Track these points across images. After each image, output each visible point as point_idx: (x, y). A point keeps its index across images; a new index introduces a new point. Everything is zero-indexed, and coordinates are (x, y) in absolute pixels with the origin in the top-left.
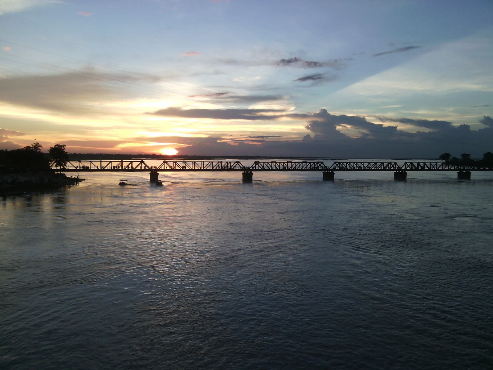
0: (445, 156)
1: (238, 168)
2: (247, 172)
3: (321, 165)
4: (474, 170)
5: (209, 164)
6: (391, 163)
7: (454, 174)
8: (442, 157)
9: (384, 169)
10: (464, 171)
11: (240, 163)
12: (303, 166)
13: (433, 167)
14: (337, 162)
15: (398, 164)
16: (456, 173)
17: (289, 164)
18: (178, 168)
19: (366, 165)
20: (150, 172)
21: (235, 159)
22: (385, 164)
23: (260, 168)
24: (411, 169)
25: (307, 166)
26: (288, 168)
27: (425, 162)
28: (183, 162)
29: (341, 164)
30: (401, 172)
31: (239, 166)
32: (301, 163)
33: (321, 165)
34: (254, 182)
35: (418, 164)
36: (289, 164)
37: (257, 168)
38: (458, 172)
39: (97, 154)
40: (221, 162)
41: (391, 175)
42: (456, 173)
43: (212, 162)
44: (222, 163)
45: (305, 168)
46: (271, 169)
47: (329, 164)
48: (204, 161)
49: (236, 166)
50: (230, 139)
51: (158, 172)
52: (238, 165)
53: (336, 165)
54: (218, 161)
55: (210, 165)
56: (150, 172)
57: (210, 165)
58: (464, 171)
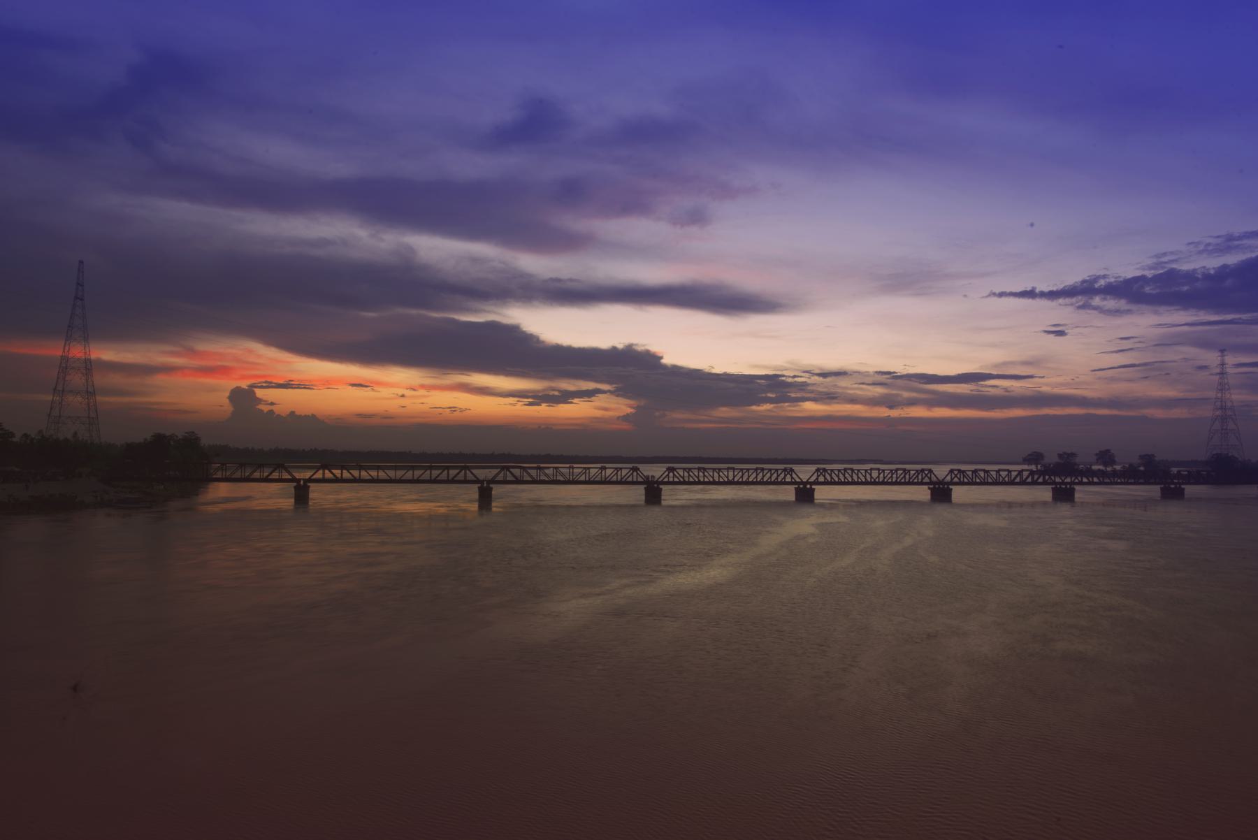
0: (1035, 458)
1: (671, 479)
2: (805, 486)
3: (929, 475)
4: (1081, 483)
5: (741, 473)
6: (923, 471)
7: (1045, 493)
8: (1027, 460)
9: (1012, 483)
10: (1173, 486)
11: (639, 469)
12: (764, 476)
13: (1004, 479)
14: (956, 470)
15: (935, 473)
16: (1157, 488)
17: (731, 474)
18: (990, 480)
19: (875, 474)
20: (645, 486)
21: (843, 464)
22: (1014, 474)
23: (721, 480)
24: (961, 483)
25: (757, 475)
26: (871, 477)
27: (854, 468)
28: (570, 468)
29: (829, 472)
30: (1064, 486)
31: (674, 475)
32: (902, 472)
33: (929, 475)
34: (816, 501)
35: (975, 472)
36: (731, 474)
37: (821, 479)
38: (795, 488)
39: (311, 449)
40: (605, 468)
41: (923, 493)
42: (1157, 488)
43: (621, 469)
44: (607, 470)
45: (902, 479)
46: (869, 480)
47: (941, 471)
48: (575, 465)
49: (668, 475)
50: (533, 391)
51: (661, 486)
52: (635, 474)
53: (924, 475)
54: (631, 466)
55: (617, 473)
56: (645, 486)
57: (617, 473)
58: (1173, 486)
